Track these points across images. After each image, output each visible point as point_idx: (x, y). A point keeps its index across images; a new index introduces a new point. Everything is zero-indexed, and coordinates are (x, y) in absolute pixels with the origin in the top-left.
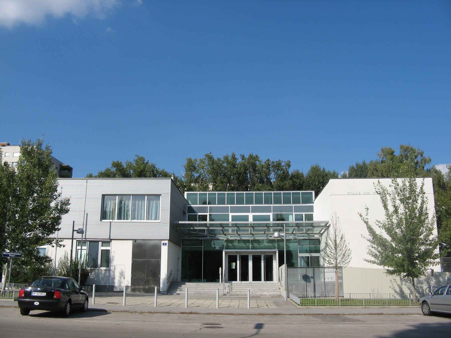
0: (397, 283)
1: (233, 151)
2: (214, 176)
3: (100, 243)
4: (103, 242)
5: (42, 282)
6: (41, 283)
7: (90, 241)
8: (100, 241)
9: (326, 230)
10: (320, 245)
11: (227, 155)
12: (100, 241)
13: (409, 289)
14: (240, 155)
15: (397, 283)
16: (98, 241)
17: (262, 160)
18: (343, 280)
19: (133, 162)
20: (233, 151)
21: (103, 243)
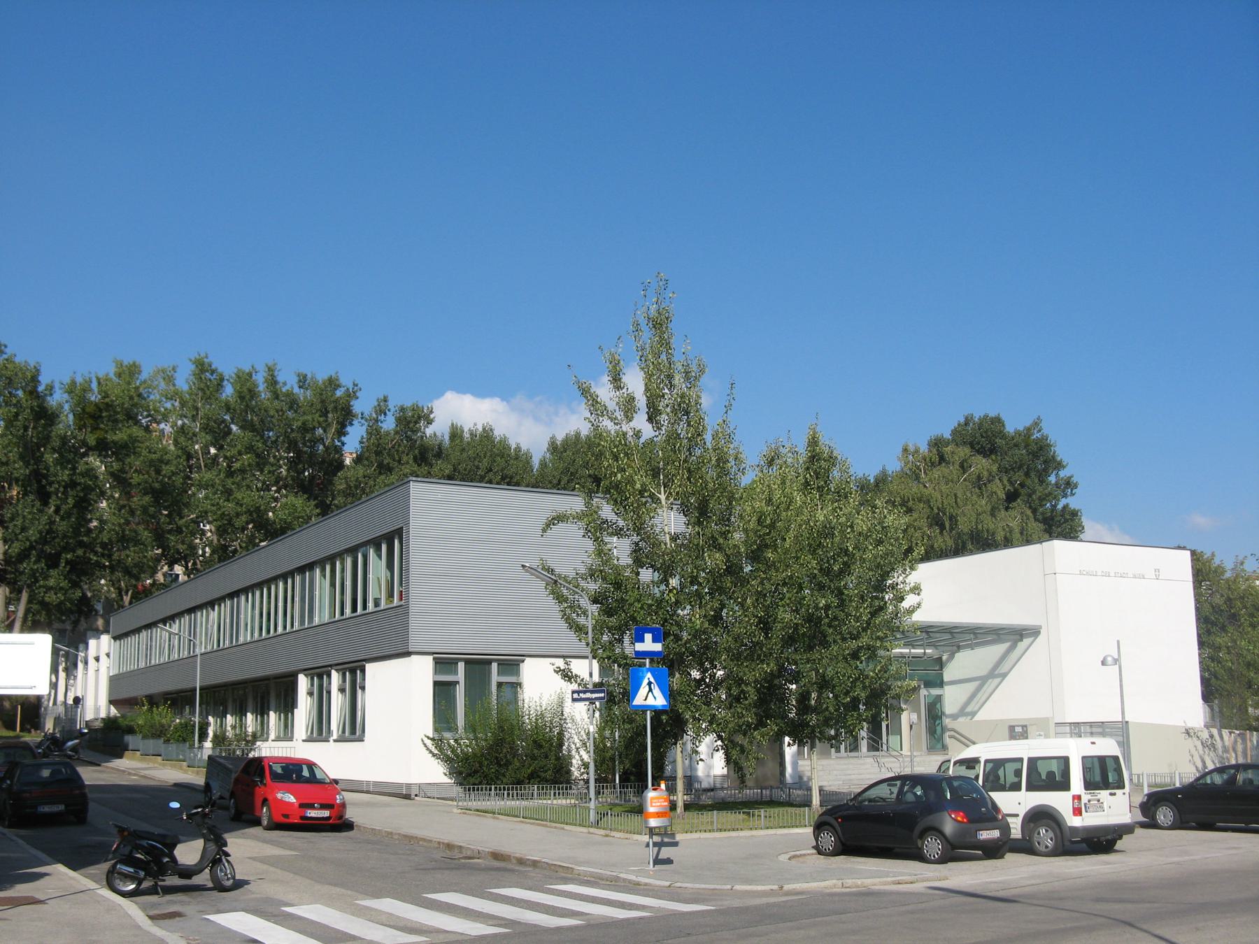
0: (1198, 753)
1: (274, 360)
2: (818, 498)
3: (494, 666)
4: (501, 664)
5: (18, 708)
6: (19, 707)
7: (467, 662)
8: (461, 660)
9: (1003, 641)
10: (942, 670)
11: (253, 367)
12: (461, 660)
13: (1213, 762)
14: (295, 372)
15: (1198, 753)
16: (489, 662)
17: (178, 370)
18: (572, 696)
19: (466, 430)
20: (274, 360)
21: (501, 664)
